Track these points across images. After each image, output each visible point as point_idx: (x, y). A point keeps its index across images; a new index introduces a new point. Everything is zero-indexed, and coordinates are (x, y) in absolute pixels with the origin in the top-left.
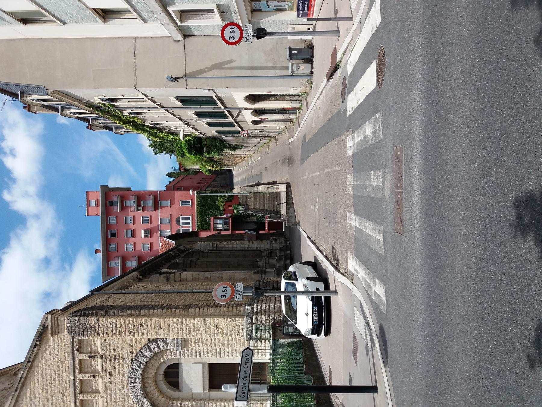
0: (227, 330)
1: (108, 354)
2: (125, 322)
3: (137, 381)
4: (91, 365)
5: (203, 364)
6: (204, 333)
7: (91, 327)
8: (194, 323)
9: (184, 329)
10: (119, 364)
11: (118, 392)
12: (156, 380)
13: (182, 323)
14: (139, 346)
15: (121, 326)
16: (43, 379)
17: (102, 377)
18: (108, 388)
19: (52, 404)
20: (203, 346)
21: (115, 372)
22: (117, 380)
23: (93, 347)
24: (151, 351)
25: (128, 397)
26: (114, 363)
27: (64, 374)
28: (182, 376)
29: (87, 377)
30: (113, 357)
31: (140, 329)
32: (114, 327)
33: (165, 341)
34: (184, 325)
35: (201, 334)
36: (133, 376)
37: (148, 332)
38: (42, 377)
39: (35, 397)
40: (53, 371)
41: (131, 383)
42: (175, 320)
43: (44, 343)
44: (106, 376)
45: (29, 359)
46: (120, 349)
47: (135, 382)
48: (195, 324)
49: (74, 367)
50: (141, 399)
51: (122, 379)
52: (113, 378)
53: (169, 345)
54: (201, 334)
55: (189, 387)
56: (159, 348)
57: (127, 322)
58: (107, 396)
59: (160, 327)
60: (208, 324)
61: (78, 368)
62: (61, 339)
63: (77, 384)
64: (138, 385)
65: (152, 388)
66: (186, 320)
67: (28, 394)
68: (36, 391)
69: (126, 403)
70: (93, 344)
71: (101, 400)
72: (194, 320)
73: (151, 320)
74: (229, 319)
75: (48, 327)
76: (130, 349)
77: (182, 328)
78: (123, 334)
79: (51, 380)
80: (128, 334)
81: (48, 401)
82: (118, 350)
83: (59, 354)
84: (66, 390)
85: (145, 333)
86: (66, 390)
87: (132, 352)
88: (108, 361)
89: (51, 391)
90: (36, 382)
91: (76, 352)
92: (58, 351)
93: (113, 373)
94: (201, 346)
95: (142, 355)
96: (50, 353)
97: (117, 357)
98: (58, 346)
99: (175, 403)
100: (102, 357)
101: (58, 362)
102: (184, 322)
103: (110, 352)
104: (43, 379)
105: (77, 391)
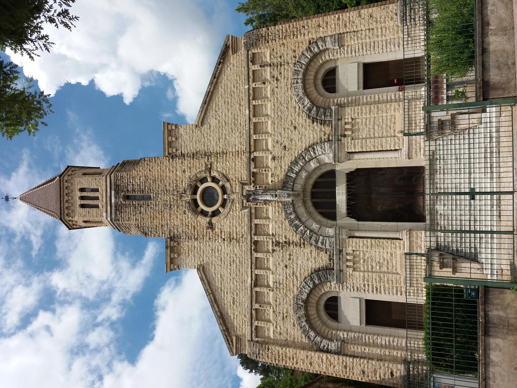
0: (380, 18)
1: (275, 61)
2: (289, 26)
3: (299, 81)
4: (262, 75)
5: (360, 299)
6: (359, 25)
7: (262, 36)
8: (350, 17)
9: (341, 24)
10: (285, 69)
11: (283, 94)
12: (318, 303)
13: (339, 19)
14: (301, 50)
15: (286, 31)
19: (232, 113)
20: (358, 40)
21: (281, 77)
22: (283, 84)
23: (263, 59)
24: (311, 51)
25: (292, 98)
26: (280, 69)
28: (338, 78)
29: (258, 85)
30: (279, 64)
31: (302, 31)
32: (281, 33)
33: (323, 39)
34: (341, 20)
35: (357, 26)
36: (296, 77)
37: (309, 32)
39: (219, 109)
40: (232, 85)
42: (332, 17)
43: (226, 61)
45: (215, 75)
46: (285, 56)
47: (297, 83)
48: (351, 17)
49: (249, 77)
52: (279, 82)
53: (327, 44)
54: (357, 26)
56: (318, 48)
57: (291, 26)
59: (319, 26)
60: (363, 16)
63: (251, 92)
64: (300, 85)
65: (312, 89)
66: (342, 16)
67: (214, 108)
68: (220, 104)
69: (290, 104)
70: (264, 56)
71: (269, 105)
72: (350, 13)
73: (312, 21)
74: (382, 7)
75: (229, 47)
76: (294, 54)
77: (339, 24)
78: (288, 37)
80: (292, 36)
81: (228, 111)
83: (238, 69)
84: (242, 100)
85: (306, 33)
86: (242, 100)
87: (295, 57)
88: (275, 68)
89: (231, 103)
91: (250, 63)
93: (279, 78)
94: (356, 40)
95: (303, 57)
96: (231, 70)
97: (283, 64)
98: (236, 62)
99: (332, 100)
100: (270, 65)
101: (237, 77)
102: (341, 17)
103: (277, 59)
105: (251, 98)
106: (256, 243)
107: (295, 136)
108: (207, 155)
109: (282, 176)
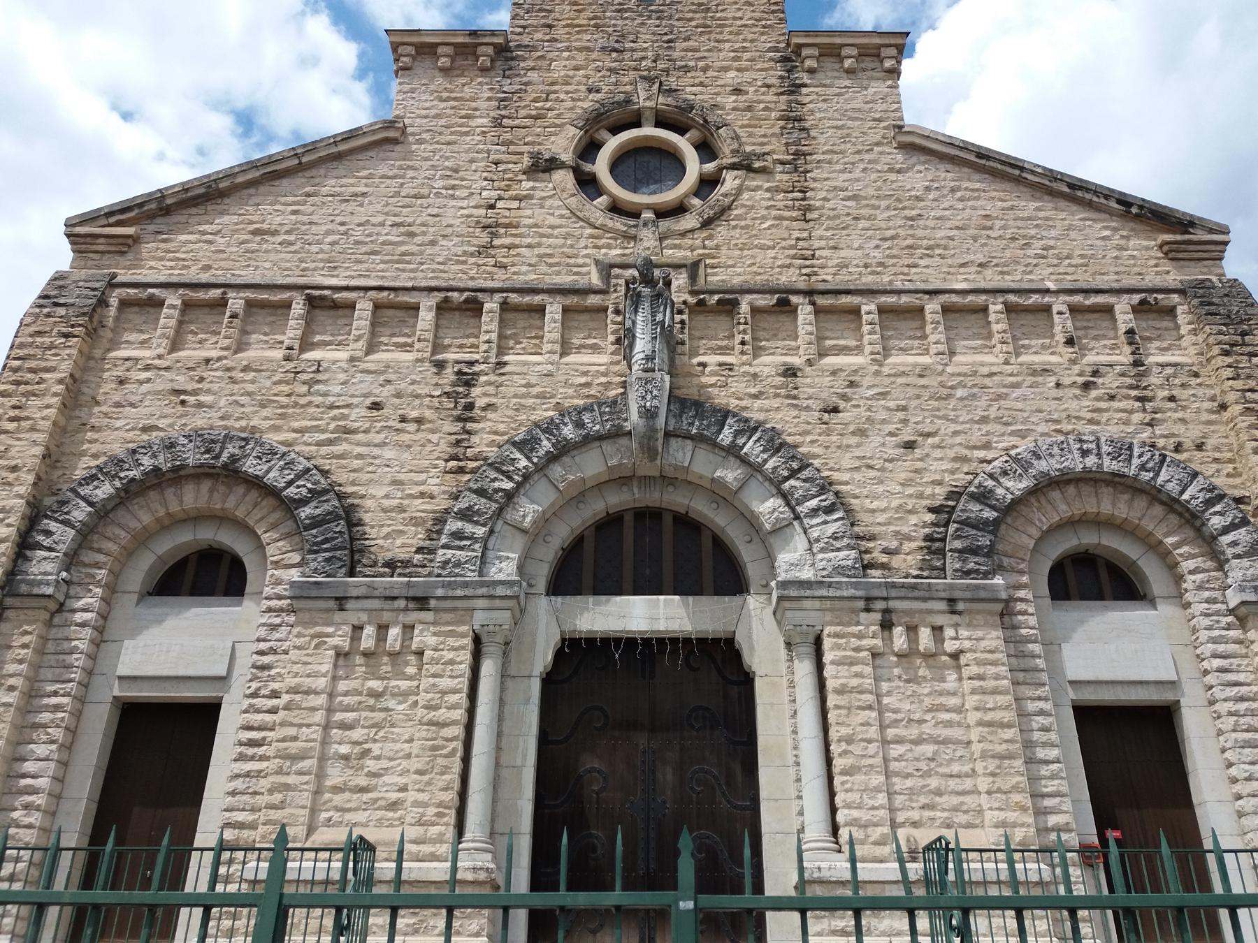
1: (1154, 380)
7: (1243, 334)
10: (1131, 412)
14: (1209, 469)
16: (1022, 219)
17: (1073, 362)
18: (1040, 379)
21: (1098, 399)
23: (1157, 344)
25: (1022, 435)
26: (1127, 397)
27: (1051, 270)
38: (1029, 218)
40: (1052, 243)
41: (1081, 441)
43: (1132, 224)
44: (1080, 375)
45: (1080, 188)
47: (1084, 453)
49: (1087, 292)
50: (1033, 472)
51: (1078, 418)
52: (1078, 392)
53: (1245, 562)
55: (1074, 630)
58: (1011, 375)
61: (1087, 303)
62: (1156, 266)
63: (1035, 298)
64: (1076, 463)
65: (1063, 507)
68: (980, 203)
70: (1165, 344)
79: (1024, 237)
81: (958, 228)
82: (1175, 411)
86: (1002, 273)
87: (1178, 448)
88: (1129, 381)
89: (989, 237)
90: (1010, 203)
91: (1136, 298)
92: (1116, 258)
93: (1094, 393)
97: (1148, 405)
100: (1137, 363)
101: (1082, 256)
103: (1161, 387)
104: (1022, 219)
105: (1012, 298)
106: (473, 308)
107: (877, 446)
108: (798, 161)
109: (722, 398)
